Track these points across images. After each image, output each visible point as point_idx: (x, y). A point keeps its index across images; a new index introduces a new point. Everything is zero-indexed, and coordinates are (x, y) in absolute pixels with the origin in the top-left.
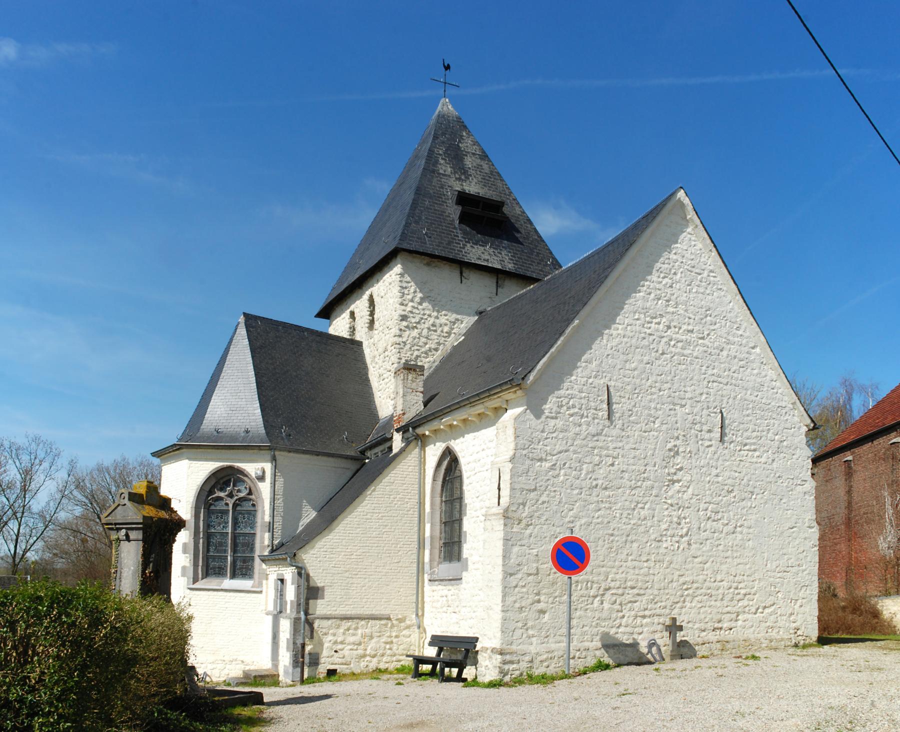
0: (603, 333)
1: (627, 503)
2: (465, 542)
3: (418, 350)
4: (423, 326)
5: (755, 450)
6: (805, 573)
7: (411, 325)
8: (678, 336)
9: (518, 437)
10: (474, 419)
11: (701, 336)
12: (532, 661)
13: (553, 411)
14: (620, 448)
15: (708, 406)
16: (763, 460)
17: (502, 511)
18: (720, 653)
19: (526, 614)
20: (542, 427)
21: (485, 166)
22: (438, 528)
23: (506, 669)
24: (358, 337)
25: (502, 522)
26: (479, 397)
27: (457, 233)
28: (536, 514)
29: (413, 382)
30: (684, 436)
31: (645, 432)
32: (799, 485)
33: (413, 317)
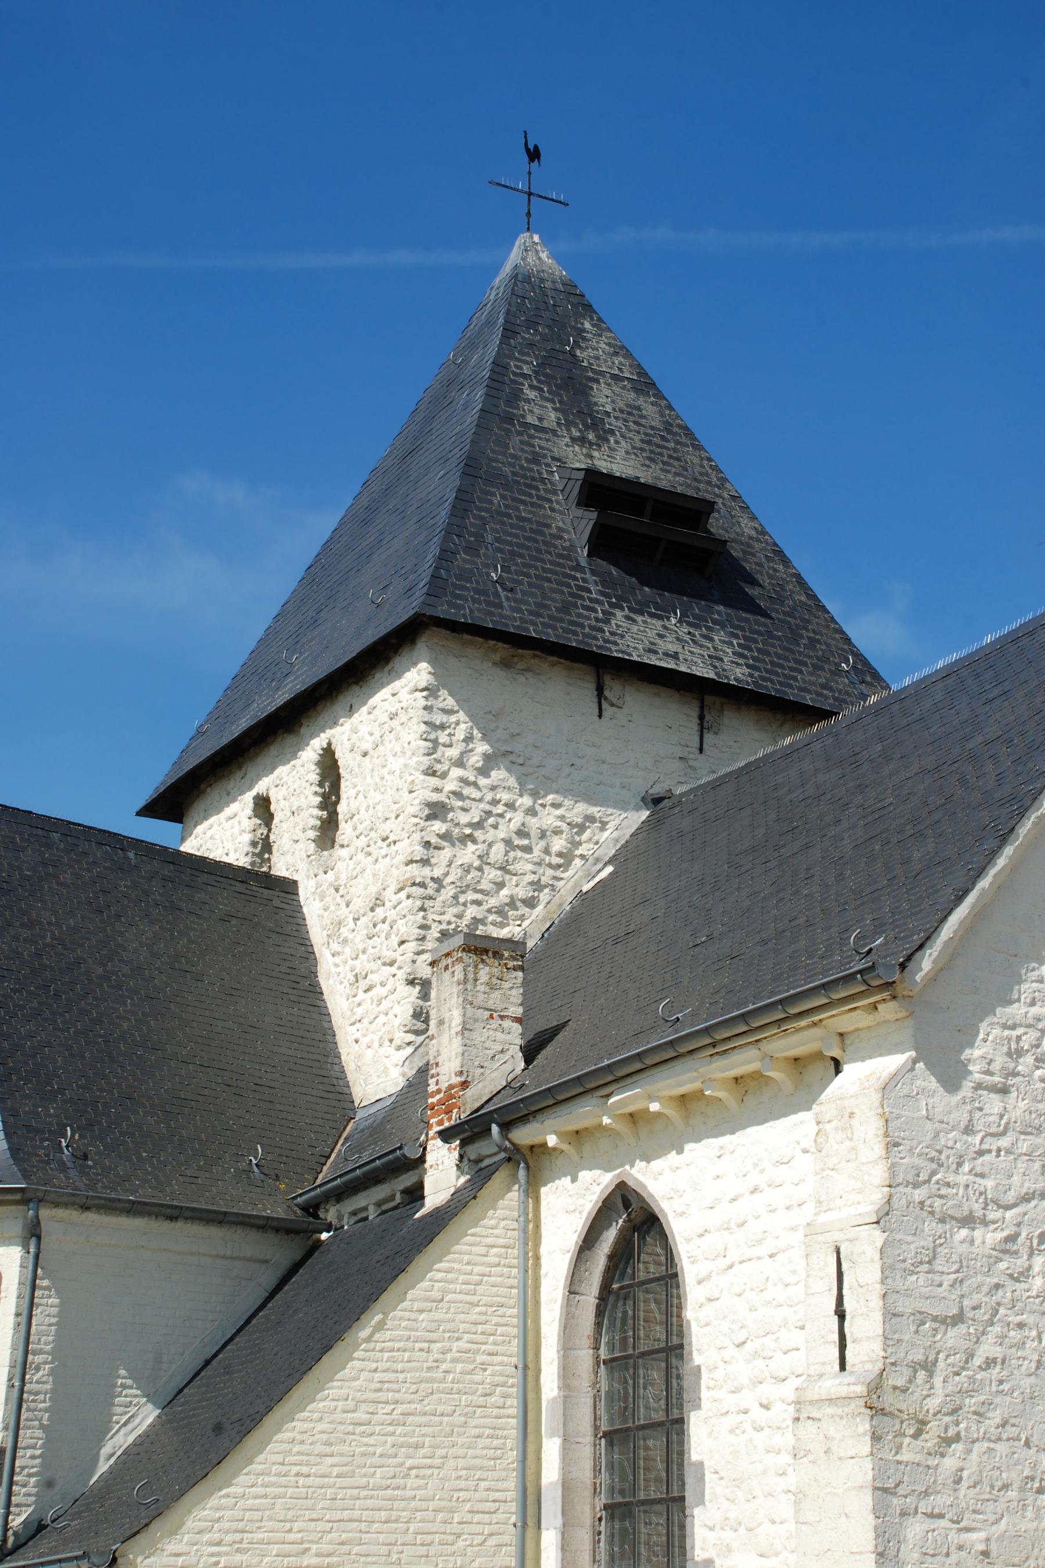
2: (701, 1502)
3: (478, 903)
4: (491, 835)
9: (897, 1145)
13: (996, 1067)
17: (860, 1389)
20: (966, 1117)
21: (650, 410)
22: (585, 1452)
24: (280, 867)
25: (864, 1426)
27: (584, 580)
28: (971, 1403)
29: (493, 988)
33: (465, 810)
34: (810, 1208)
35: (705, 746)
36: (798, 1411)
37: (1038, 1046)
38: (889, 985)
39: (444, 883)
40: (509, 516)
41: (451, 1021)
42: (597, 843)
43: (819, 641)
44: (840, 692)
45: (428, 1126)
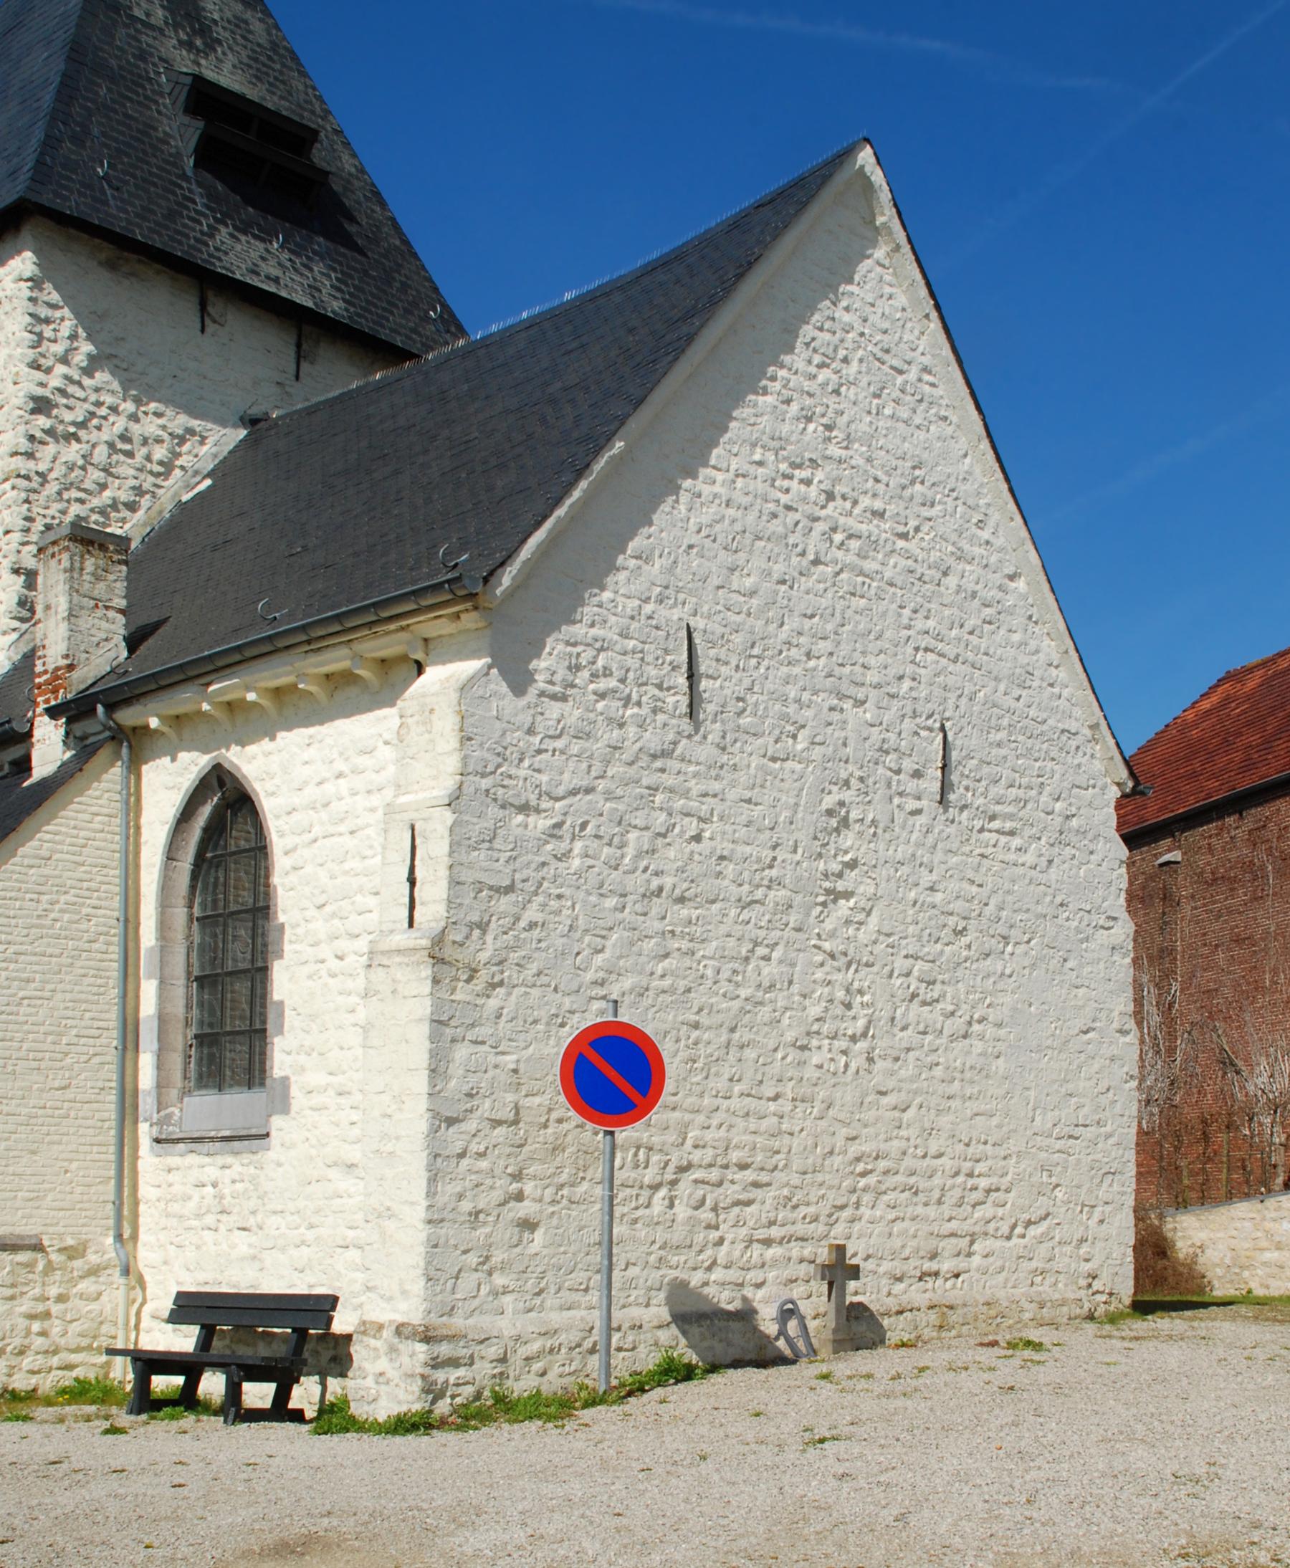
0: (679, 487)
1: (731, 943)
3: (82, 501)
4: (94, 436)
5: (1012, 833)
6: (1111, 1141)
7: (61, 428)
8: (850, 522)
9: (470, 739)
10: (313, 688)
11: (901, 529)
12: (503, 1360)
13: (558, 678)
14: (715, 796)
15: (914, 712)
16: (1029, 858)
17: (425, 942)
18: (935, 1334)
19: (488, 1230)
20: (530, 719)
21: (257, 27)
23: (440, 1381)
25: (427, 972)
26: (240, 652)
27: (190, 191)
28: (514, 957)
29: (98, 579)
30: (861, 779)
31: (774, 759)
32: (1102, 927)
34: (389, 794)
35: (301, 374)
36: (370, 959)
37: (594, 663)
38: (472, 596)
39: (49, 478)
40: (116, 112)
41: (57, 606)
42: (196, 456)
43: (410, 287)
44: (427, 338)
45: (36, 704)
